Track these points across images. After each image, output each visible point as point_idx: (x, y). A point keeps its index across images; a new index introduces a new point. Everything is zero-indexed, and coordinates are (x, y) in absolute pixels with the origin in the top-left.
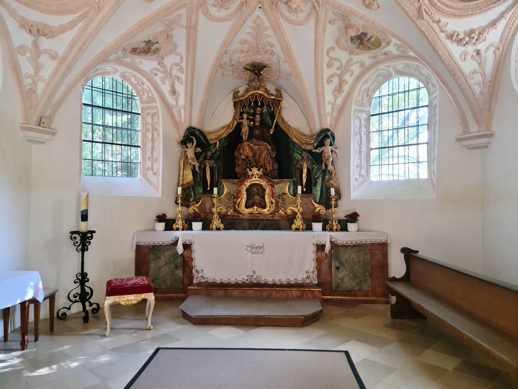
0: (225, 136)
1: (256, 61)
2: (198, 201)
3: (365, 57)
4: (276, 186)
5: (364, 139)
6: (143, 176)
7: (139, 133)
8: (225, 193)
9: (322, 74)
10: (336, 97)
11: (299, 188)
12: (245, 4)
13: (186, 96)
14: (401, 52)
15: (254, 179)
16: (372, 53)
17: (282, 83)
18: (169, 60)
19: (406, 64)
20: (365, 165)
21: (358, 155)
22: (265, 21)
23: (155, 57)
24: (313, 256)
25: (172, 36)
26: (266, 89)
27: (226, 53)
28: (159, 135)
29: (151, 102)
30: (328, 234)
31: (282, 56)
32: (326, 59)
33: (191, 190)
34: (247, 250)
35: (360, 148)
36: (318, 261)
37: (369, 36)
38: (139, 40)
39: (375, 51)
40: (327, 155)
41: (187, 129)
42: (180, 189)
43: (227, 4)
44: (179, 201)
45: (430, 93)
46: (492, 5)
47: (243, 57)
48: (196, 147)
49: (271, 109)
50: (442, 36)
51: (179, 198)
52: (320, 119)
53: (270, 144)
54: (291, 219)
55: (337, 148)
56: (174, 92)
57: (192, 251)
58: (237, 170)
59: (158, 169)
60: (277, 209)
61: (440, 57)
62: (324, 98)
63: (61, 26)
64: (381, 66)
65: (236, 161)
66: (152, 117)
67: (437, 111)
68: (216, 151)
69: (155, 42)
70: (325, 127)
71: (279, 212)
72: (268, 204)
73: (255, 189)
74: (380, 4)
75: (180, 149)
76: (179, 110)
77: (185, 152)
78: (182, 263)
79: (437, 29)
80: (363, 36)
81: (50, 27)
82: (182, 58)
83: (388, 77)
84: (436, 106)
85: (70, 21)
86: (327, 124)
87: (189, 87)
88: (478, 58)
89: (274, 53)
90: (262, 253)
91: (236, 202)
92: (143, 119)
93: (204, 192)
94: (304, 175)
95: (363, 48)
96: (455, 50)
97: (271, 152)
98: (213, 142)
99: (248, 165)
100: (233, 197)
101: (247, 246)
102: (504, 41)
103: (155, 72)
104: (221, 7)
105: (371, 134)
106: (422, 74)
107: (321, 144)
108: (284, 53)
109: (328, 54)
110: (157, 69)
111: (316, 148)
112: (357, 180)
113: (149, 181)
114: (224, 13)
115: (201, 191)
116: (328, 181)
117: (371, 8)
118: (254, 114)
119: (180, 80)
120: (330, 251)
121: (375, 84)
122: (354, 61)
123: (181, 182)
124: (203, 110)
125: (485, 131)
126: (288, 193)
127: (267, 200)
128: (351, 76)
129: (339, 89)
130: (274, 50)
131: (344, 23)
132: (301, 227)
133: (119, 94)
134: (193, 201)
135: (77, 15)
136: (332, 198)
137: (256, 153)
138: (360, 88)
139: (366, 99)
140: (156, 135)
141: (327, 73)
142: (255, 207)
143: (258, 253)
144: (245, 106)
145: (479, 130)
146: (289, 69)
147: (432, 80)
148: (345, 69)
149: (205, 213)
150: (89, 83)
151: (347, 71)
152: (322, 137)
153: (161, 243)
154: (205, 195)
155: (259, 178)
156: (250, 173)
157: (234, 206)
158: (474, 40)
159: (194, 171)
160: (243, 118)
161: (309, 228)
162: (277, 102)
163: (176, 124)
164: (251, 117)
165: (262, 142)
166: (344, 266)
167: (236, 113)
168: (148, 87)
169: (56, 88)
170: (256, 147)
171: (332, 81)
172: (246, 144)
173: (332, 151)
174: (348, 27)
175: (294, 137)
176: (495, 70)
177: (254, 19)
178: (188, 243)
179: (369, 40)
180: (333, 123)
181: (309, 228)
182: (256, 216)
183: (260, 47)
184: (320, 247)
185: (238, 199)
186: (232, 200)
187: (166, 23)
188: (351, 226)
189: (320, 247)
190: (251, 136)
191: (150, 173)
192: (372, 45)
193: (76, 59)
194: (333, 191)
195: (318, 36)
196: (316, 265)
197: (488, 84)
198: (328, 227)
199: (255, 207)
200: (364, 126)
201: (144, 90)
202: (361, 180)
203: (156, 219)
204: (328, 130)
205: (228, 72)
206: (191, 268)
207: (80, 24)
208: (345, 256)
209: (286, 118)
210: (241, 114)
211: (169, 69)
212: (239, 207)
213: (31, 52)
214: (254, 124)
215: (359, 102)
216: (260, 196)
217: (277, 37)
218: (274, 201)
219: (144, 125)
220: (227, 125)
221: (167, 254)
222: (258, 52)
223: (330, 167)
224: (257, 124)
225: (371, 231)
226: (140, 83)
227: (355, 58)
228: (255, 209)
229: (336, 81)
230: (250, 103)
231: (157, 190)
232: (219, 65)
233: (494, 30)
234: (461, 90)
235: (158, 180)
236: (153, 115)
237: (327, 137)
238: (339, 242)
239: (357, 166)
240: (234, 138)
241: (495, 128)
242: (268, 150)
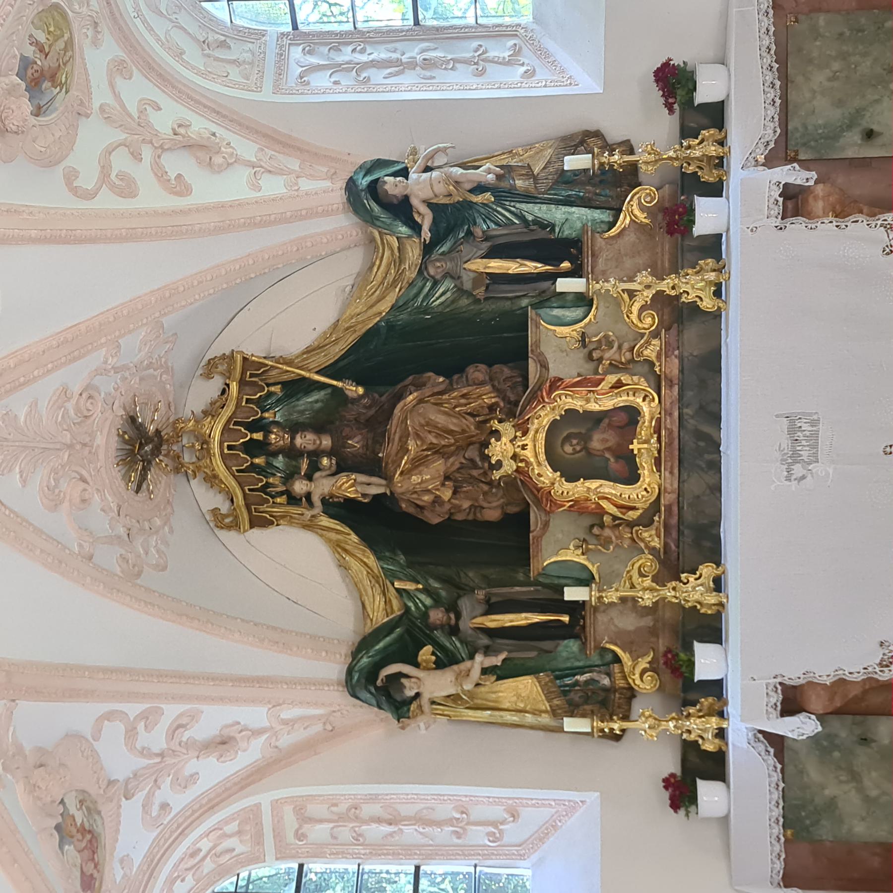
0: (371, 560)
1: (113, 453)
2: (609, 657)
3: (96, 58)
4: (553, 373)
5: (380, 53)
6: (522, 857)
7: (367, 868)
8: (582, 560)
9: (156, 213)
11: (564, 285)
13: (236, 701)
15: (528, 454)
16: (81, 34)
17: (183, 357)
18: (118, 761)
20: (475, 44)
21: (440, 75)
23: (106, 810)
24: (827, 227)
25: (41, 751)
26: (206, 413)
27: (90, 558)
28: (373, 798)
29: (259, 825)
30: (738, 176)
31: (95, 359)
32: (107, 201)
33: (568, 681)
34: (803, 477)
35: (412, 65)
36: (842, 210)
37: (30, 51)
39: (75, 26)
40: (440, 189)
42: (571, 724)
44: (616, 726)
48: (417, 665)
49: (270, 394)
51: (606, 727)
53: (400, 397)
54: (676, 313)
55: (414, 152)
56: (224, 743)
57: (810, 683)
58: (492, 514)
59: (498, 801)
60: (639, 368)
65: (459, 517)
68: (427, 591)
69: (61, 809)
70: (339, 196)
71: (653, 357)
72: (621, 400)
73: (568, 449)
75: (421, 723)
76: (285, 722)
77: (433, 703)
78: (849, 718)
80: (30, 72)
82: (109, 716)
89: (87, 387)
90: (814, 423)
91: (615, 518)
92: (318, 853)
93: (576, 637)
94: (513, 267)
97: (427, 391)
98: (395, 603)
99: (475, 473)
100: (596, 531)
101: (788, 479)
107: (401, 209)
109: (90, 195)
111: (416, 228)
112: (530, 74)
113: (542, 836)
115: (573, 645)
116: (535, 178)
118: (292, 453)
119: (184, 721)
120: (806, 165)
122: (110, 100)
123: (545, 719)
124: (280, 637)
126: (577, 327)
127: (608, 403)
129: (203, 150)
130: (76, 389)
132: (712, 276)
134: (609, 674)
136: (602, 164)
137: (431, 447)
140: (375, 809)
141: (152, 197)
142: (635, 446)
143: (814, 437)
148: (137, 134)
149: (653, 632)
151: (143, 123)
152: (376, 208)
153: (776, 795)
154: (590, 630)
155: (525, 433)
156: (509, 467)
157: (631, 525)
159: (503, 673)
161: (713, 246)
162: (250, 372)
163: (332, 734)
165: (394, 424)
166: (859, 113)
167: (291, 520)
170: (412, 445)
171: (179, 176)
172: (401, 485)
173: (427, 169)
175: (375, 309)
178: (777, 698)
179: (42, 50)
181: (713, 246)
182: (669, 444)
183: (67, 438)
184: (790, 205)
185: (602, 512)
186: (607, 532)
188: (707, 91)
189: (794, 202)
190: (371, 465)
191: (513, 833)
194: (574, 162)
195: (33, 233)
196: (860, 217)
198: (708, 177)
199: (635, 446)
200: (333, 54)
201: (219, 849)
202: (528, 58)
203: (682, 812)
206: (872, 686)
208: (820, 110)
210: (293, 500)
211: (145, 762)
212: (634, 508)
214: (330, 454)
216: (590, 430)
218: (612, 379)
220: (335, 551)
221: (814, 773)
222: (85, 445)
223: (486, 173)
224: (326, 442)
225: (725, 16)
227: (101, 96)
228: (643, 447)
229: (178, 164)
230: (253, 468)
231: (572, 808)
232: (130, 582)
235: (538, 803)
236: (304, 819)
237: (374, 188)
238: (770, 132)
239: (481, 73)
240: (378, 524)
242: (421, 401)
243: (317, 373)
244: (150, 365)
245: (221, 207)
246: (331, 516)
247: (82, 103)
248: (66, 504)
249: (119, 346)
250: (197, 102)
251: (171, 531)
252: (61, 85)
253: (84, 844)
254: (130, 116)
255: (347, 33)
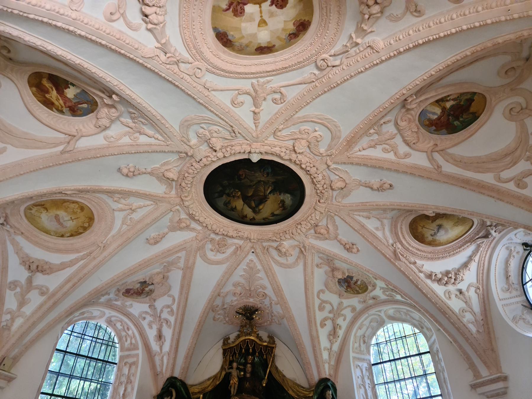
0: (210, 388)
1: (248, 304)
3: (355, 301)
9: (315, 316)
10: (332, 344)
12: (239, 249)
13: (172, 340)
14: (388, 296)
16: (361, 297)
17: (275, 328)
18: (160, 304)
19: (395, 308)
22: (257, 264)
25: (168, 278)
26: (258, 334)
27: (219, 295)
28: (133, 389)
31: (274, 298)
32: (317, 302)
37: (355, 279)
38: (134, 281)
41: (168, 379)
43: (223, 248)
45: (428, 339)
46: (459, 250)
47: (235, 301)
50: (422, 275)
52: (318, 367)
61: (426, 296)
62: (319, 343)
63: (62, 264)
64: (373, 311)
66: (130, 367)
67: (441, 356)
70: (324, 376)
74: (360, 249)
76: (162, 357)
79: (416, 271)
81: (51, 264)
82: (174, 300)
83: (381, 324)
84: (438, 351)
85: (73, 260)
86: (326, 372)
87: (177, 330)
88: (461, 296)
92: (119, 370)
95: (352, 292)
96: (439, 289)
102: (481, 281)
103: (144, 315)
104: (218, 251)
105: (377, 387)
106: (414, 319)
108: (275, 294)
109: (318, 297)
110: (146, 313)
114: (220, 257)
117: (352, 252)
118: (245, 364)
119: (169, 324)
121: (370, 330)
122: (345, 305)
124: (189, 357)
125: (497, 374)
128: (344, 320)
129: (333, 333)
131: (330, 267)
133: (99, 341)
135: (82, 254)
138: (355, 334)
139: (363, 347)
140: (129, 389)
141: (319, 316)
144: (235, 353)
145: (491, 373)
146: (281, 312)
147: (426, 324)
148: (336, 313)
150: (70, 328)
151: (339, 315)
152: (321, 388)
158: (453, 281)
160: (232, 368)
162: (270, 349)
163: (156, 375)
164: (241, 367)
167: (224, 362)
168: (133, 333)
169: (34, 325)
171: (325, 325)
174: (334, 269)
175: (290, 389)
176: (483, 309)
177: (248, 263)
180: (332, 373)
183: (252, 289)
187: (165, 264)
190: (240, 390)
192: (359, 288)
193: (66, 295)
197: (482, 322)
201: (128, 337)
204: (327, 380)
205: (219, 316)
207: (82, 262)
209: (280, 368)
211: (159, 311)
213: (21, 288)
214: (244, 375)
215: (356, 348)
217: (268, 279)
219: (117, 377)
220: (214, 376)
224: (248, 375)
226: (126, 328)
232: (211, 308)
233: (468, 272)
234: (456, 328)
236: (131, 365)
237: (327, 388)
241: (506, 370)
243: (270, 371)
244: (272, 316)
245: (318, 337)
246: (225, 375)
247: (343, 296)
248: (234, 288)
249: (277, 304)
250: (347, 333)
251: (224, 323)
252: (347, 289)
253: (139, 290)
254: (341, 311)
255: (374, 382)
